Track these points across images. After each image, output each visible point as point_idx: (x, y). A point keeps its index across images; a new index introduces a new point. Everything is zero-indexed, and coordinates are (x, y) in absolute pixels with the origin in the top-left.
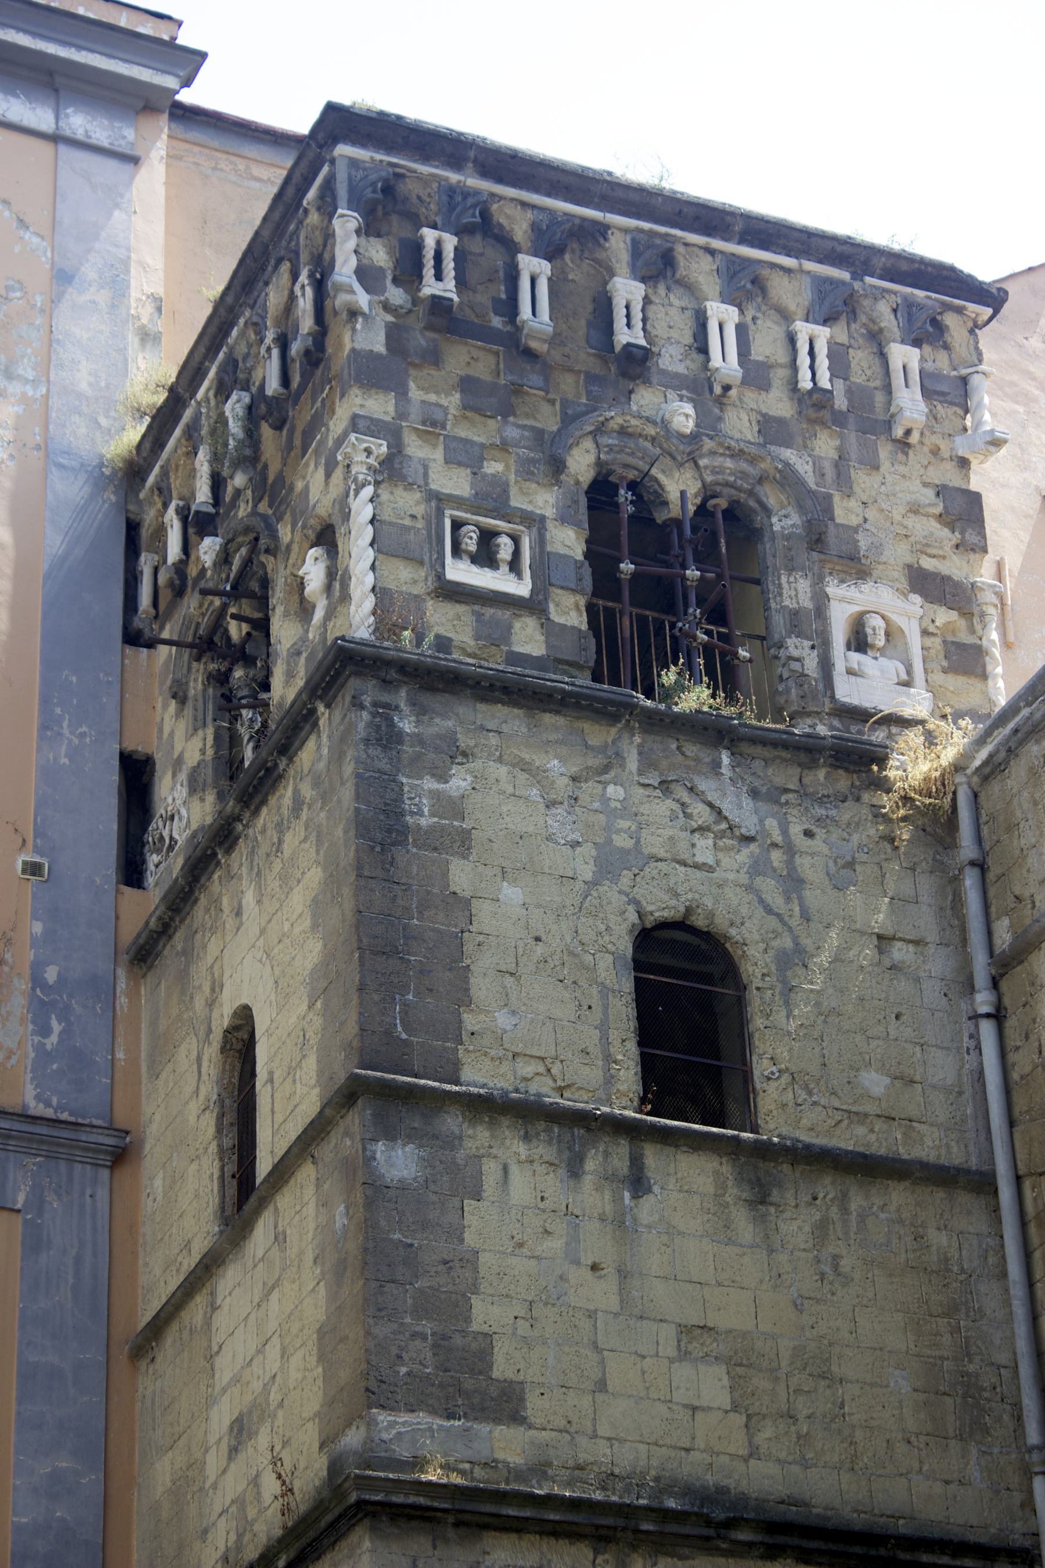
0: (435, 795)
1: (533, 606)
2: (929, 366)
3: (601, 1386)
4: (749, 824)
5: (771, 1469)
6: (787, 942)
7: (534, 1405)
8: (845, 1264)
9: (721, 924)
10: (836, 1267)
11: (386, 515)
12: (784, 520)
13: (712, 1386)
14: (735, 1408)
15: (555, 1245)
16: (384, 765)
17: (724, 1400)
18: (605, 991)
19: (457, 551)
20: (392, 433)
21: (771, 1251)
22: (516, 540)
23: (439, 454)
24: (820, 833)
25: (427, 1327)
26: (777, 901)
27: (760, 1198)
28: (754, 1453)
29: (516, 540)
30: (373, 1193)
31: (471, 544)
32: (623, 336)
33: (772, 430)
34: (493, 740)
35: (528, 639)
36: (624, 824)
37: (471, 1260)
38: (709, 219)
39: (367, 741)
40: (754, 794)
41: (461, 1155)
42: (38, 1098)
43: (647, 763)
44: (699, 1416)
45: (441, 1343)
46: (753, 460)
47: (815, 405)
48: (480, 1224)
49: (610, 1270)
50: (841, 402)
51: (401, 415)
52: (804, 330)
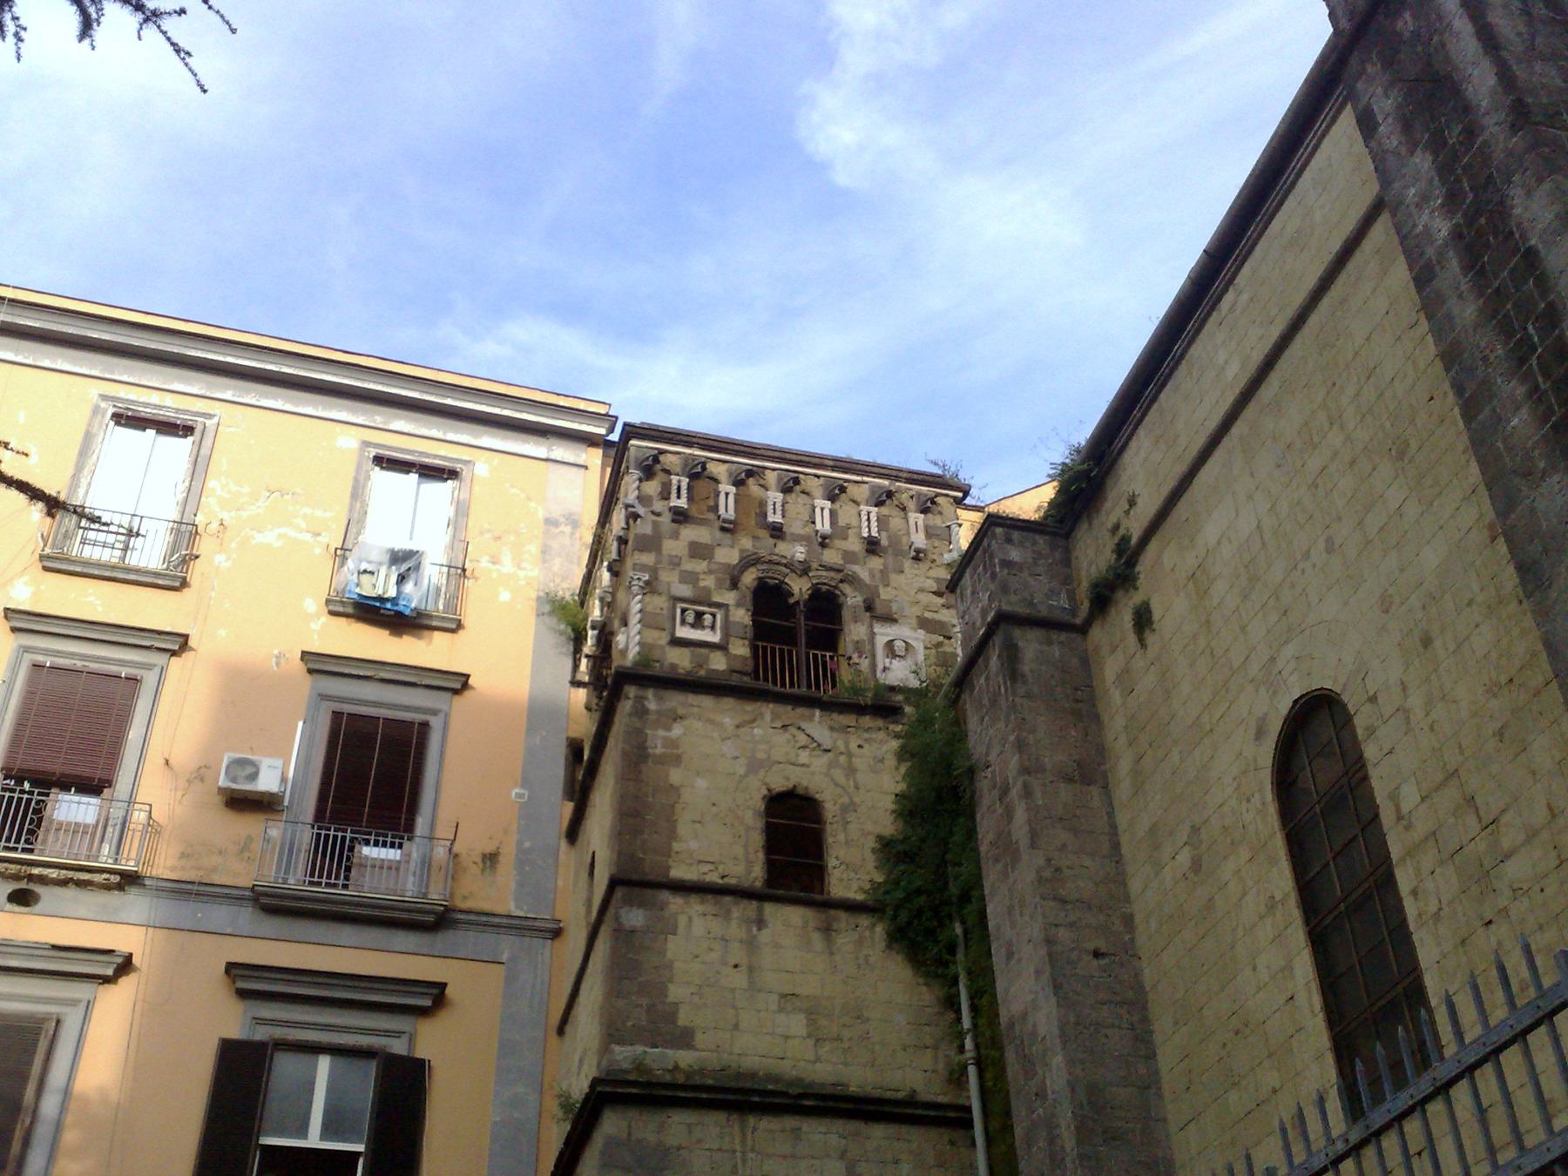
0: (665, 738)
1: (721, 647)
2: (931, 523)
3: (736, 1027)
4: (827, 744)
5: (829, 1068)
6: (846, 800)
7: (700, 1038)
8: (872, 960)
9: (812, 792)
10: (867, 962)
11: (649, 608)
12: (852, 599)
13: (797, 1024)
14: (809, 1036)
15: (715, 956)
16: (638, 725)
17: (804, 1032)
18: (748, 829)
19: (683, 622)
20: (654, 571)
21: (832, 954)
22: (714, 616)
23: (676, 579)
24: (866, 746)
25: (644, 1002)
26: (842, 780)
27: (827, 930)
28: (818, 1059)
29: (714, 616)
30: (624, 936)
31: (690, 618)
32: (771, 519)
33: (849, 557)
34: (696, 710)
35: (718, 663)
36: (763, 747)
37: (670, 966)
38: (816, 461)
39: (630, 715)
40: (832, 729)
41: (666, 913)
42: (517, 907)
43: (775, 717)
44: (790, 1042)
45: (650, 1009)
46: (840, 571)
47: (872, 546)
48: (674, 947)
49: (743, 968)
50: (884, 542)
51: (658, 562)
52: (864, 508)
